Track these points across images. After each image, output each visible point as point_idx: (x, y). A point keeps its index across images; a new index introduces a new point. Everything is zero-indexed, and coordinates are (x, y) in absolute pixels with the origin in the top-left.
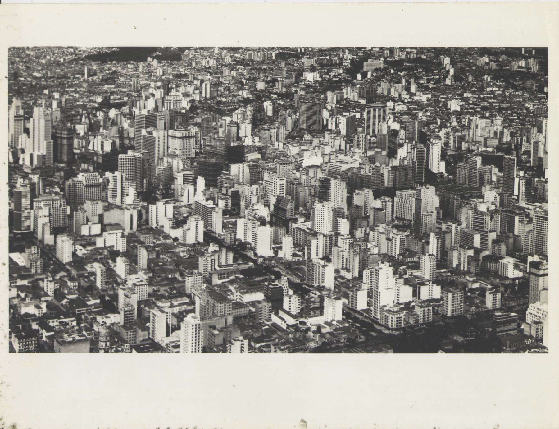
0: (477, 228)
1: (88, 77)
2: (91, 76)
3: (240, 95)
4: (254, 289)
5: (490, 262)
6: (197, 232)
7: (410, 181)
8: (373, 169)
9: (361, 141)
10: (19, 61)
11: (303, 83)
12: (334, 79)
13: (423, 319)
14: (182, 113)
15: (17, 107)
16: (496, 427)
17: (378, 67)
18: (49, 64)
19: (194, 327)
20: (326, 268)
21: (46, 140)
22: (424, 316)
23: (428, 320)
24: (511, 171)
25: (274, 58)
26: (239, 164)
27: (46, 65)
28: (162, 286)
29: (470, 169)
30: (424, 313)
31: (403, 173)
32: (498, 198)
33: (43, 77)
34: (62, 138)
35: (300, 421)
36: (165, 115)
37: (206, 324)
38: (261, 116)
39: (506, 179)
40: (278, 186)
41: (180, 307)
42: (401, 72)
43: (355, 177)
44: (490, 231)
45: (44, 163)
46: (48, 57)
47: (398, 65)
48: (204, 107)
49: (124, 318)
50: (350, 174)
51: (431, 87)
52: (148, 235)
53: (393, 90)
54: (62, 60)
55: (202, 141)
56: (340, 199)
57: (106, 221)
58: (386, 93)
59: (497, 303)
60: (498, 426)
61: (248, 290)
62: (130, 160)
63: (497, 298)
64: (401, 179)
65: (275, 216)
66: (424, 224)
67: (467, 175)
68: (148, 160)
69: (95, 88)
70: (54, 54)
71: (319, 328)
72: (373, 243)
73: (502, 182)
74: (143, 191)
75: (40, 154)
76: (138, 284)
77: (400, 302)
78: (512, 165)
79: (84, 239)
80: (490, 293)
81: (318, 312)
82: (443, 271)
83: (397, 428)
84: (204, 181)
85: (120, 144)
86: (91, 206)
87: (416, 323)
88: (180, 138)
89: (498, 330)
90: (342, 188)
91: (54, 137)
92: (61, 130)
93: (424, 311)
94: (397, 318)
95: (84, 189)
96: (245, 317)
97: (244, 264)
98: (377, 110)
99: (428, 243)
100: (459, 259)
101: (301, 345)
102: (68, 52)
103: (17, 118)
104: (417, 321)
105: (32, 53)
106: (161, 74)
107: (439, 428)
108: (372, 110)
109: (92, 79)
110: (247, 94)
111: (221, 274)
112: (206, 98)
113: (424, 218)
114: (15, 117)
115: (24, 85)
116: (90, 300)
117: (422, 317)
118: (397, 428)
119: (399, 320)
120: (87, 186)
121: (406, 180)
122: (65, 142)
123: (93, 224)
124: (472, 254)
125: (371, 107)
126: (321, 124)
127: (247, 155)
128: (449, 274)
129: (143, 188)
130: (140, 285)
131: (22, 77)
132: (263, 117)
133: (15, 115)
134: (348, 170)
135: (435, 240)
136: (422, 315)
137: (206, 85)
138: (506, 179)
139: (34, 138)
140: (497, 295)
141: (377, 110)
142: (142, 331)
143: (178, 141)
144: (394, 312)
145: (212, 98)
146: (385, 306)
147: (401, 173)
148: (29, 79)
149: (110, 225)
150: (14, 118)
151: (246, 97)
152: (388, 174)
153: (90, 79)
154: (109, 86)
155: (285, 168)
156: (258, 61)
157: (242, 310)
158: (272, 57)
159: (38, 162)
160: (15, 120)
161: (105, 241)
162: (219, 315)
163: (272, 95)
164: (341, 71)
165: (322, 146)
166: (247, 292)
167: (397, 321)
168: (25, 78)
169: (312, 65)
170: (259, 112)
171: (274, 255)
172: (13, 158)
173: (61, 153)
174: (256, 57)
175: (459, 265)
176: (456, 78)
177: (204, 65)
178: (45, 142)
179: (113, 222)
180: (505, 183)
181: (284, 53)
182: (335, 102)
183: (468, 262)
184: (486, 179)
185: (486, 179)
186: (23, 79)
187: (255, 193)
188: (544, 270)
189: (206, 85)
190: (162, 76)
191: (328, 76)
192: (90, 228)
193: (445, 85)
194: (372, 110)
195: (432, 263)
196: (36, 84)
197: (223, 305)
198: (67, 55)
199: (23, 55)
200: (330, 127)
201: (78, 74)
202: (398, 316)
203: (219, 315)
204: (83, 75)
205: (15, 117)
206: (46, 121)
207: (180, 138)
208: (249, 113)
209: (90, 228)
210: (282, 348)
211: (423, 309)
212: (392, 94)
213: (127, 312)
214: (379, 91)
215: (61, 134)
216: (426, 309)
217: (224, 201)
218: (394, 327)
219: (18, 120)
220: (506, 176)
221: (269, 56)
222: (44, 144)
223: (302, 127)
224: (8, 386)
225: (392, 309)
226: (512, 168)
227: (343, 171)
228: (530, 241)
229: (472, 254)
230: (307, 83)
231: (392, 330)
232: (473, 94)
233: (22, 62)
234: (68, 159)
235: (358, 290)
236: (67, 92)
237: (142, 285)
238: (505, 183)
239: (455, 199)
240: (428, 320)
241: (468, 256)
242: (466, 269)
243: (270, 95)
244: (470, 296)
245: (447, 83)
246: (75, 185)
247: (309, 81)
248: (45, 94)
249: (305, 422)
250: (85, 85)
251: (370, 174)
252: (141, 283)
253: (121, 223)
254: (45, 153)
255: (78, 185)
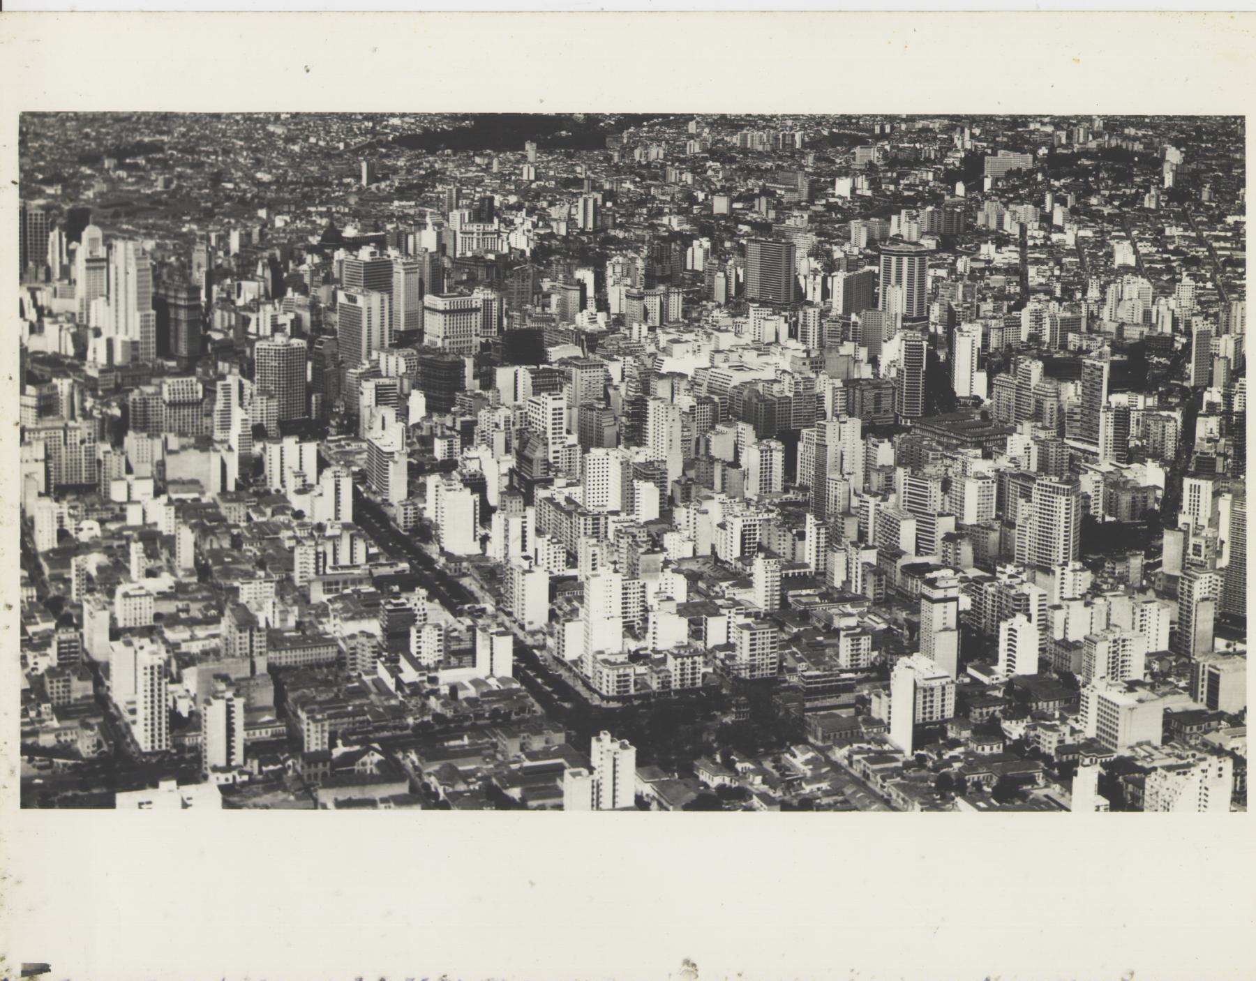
0: (914, 507)
1: (368, 184)
2: (378, 180)
3: (663, 226)
4: (368, 613)
5: (913, 578)
6: (337, 502)
7: (886, 411)
8: (797, 383)
9: (811, 325)
10: (242, 147)
11: (824, 202)
12: (906, 193)
13: (682, 680)
14: (486, 261)
15: (93, 241)
16: (1127, 977)
17: (1014, 168)
18: (311, 154)
19: (149, 671)
20: (528, 575)
21: (140, 309)
22: (682, 675)
23: (693, 684)
24: (1096, 393)
25: (798, 145)
26: (517, 367)
27: (300, 157)
28: (195, 600)
29: (1019, 388)
30: (682, 670)
31: (869, 395)
32: (1035, 450)
33: (277, 182)
34: (177, 307)
35: (680, 962)
36: (422, 265)
37: (207, 670)
38: (663, 269)
39: (1086, 412)
40: (550, 411)
41: (206, 642)
42: (1058, 180)
43: (755, 400)
44: (941, 515)
45: (135, 358)
46: (313, 140)
47: (1057, 164)
48: (568, 249)
49: (59, 654)
50: (746, 392)
51: (1106, 212)
52: (235, 505)
53: (1007, 218)
54: (341, 146)
55: (505, 321)
56: (666, 442)
57: (171, 474)
58: (993, 225)
59: (862, 657)
60: (1132, 974)
61: (357, 613)
62: (277, 352)
63: (862, 647)
64: (866, 409)
65: (518, 474)
66: (832, 498)
67: (1013, 404)
68: (334, 356)
69: (374, 207)
70: (328, 133)
71: (454, 689)
72: (686, 534)
73: (1078, 417)
74: (310, 419)
75: (127, 339)
76: (132, 593)
77: (659, 648)
78: (1097, 380)
79: (107, 509)
80: (846, 636)
81: (467, 659)
82: (804, 592)
83: (902, 979)
84: (424, 399)
85: (312, 322)
86: (135, 442)
87: (663, 687)
88: (444, 312)
89: (808, 705)
90: (670, 419)
91: (160, 304)
92: (176, 291)
93: (682, 664)
94: (619, 676)
95: (165, 411)
96: (329, 665)
97: (391, 565)
98: (905, 260)
99: (802, 536)
100: (848, 569)
101: (394, 718)
102: (359, 129)
103: (92, 265)
104: (665, 684)
105: (279, 130)
106: (532, 177)
107: (997, 980)
108: (894, 259)
109: (378, 188)
110: (680, 223)
111: (330, 584)
112: (583, 232)
113: (832, 485)
114: (88, 261)
115: (229, 198)
116: (37, 623)
117: (679, 677)
118: (902, 979)
119: (622, 681)
120: (173, 405)
121: (877, 410)
122: (182, 315)
123: (138, 478)
124: (874, 561)
125: (889, 253)
126: (792, 290)
127: (550, 349)
128: (817, 599)
129: (308, 411)
130: (135, 596)
131: (229, 181)
132: (669, 273)
133: (88, 256)
134: (744, 384)
135: (814, 530)
136: (679, 672)
137: (586, 201)
138: (1086, 412)
139: (117, 306)
140: (862, 641)
141: (905, 260)
142: (80, 679)
143: (440, 317)
144: (615, 664)
145: (596, 230)
146: (601, 652)
147: (866, 393)
148: (243, 186)
149: (174, 482)
150: (84, 264)
151: (677, 229)
152: (834, 396)
153: (373, 187)
154: (404, 203)
155: (586, 376)
156: (760, 153)
157: (323, 651)
158: (794, 142)
159: (124, 354)
160: (88, 268)
161: (144, 513)
162: (238, 653)
163: (740, 226)
164: (930, 176)
165: (716, 333)
166: (352, 618)
167: (618, 682)
168: (236, 184)
169: (871, 163)
170: (659, 260)
171: (480, 552)
172: (75, 346)
173: (177, 339)
174: (757, 139)
175: (847, 582)
176: (1175, 194)
177: (637, 158)
178: (138, 315)
179: (187, 476)
180: (1085, 419)
181: (844, 134)
182: (863, 244)
183: (863, 575)
184: (1048, 411)
185: (1048, 411)
186: (230, 186)
187: (502, 426)
188: (946, 588)
189: (586, 201)
190: (532, 182)
191: (892, 187)
192: (129, 487)
193: (1143, 209)
194: (894, 259)
195: (769, 574)
196: (254, 197)
197: (247, 634)
198: (356, 135)
199: (259, 135)
200: (809, 298)
201: (348, 176)
202: (621, 671)
203: (238, 653)
204: (359, 178)
205: (88, 261)
206: (139, 270)
207: (444, 312)
208: (640, 263)
209: (129, 487)
210: (319, 717)
211: (679, 660)
212: (1007, 227)
213: (65, 642)
214: (981, 220)
215: (176, 297)
216: (689, 661)
217: (445, 443)
218: (611, 694)
219: (95, 268)
220: (1086, 405)
221: (788, 141)
222: (135, 319)
223: (752, 295)
224: (18, 882)
225: (612, 659)
226: (1097, 387)
227: (735, 387)
228: (1027, 538)
229: (874, 561)
230: (832, 200)
231: (608, 699)
232: (1186, 230)
233: (249, 148)
234: (189, 351)
235: (569, 621)
236: (309, 214)
237: (140, 596)
238: (1085, 419)
239: (932, 450)
240: (693, 684)
241: (863, 564)
242: (859, 592)
243: (737, 224)
244: (820, 642)
245: (1146, 205)
246: (145, 403)
247: (840, 197)
248: (260, 219)
249: (694, 965)
250: (353, 200)
251: (791, 395)
252: (138, 592)
253: (203, 481)
254: (137, 338)
255: (152, 403)
